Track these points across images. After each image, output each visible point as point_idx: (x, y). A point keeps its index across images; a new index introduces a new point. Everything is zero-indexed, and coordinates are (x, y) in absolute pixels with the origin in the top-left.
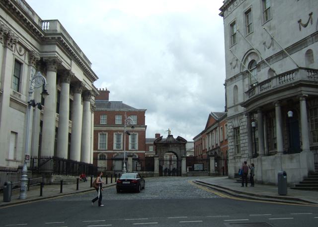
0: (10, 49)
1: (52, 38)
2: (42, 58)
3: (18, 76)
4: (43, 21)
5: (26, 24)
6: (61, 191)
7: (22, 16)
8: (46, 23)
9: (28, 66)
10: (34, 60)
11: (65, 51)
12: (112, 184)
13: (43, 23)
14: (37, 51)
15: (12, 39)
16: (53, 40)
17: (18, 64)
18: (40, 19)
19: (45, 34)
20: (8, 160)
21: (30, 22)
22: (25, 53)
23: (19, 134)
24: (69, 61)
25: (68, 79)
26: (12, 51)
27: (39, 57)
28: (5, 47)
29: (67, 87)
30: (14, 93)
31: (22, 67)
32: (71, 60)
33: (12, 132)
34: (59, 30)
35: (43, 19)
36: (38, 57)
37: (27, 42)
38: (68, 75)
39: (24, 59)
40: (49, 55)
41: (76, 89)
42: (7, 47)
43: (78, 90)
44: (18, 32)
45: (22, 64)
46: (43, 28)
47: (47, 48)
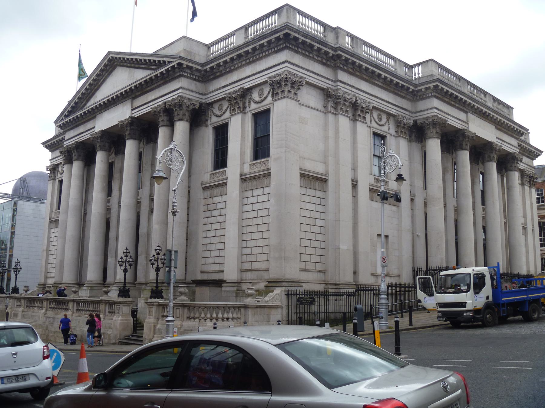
0: (362, 122)
1: (427, 89)
2: (415, 122)
5: (381, 81)
8: (417, 68)
9: (325, 113)
10: (404, 127)
15: (363, 108)
16: (428, 92)
18: (406, 65)
19: (415, 85)
22: (388, 120)
24: (462, 116)
25: (464, 143)
26: (366, 123)
29: (465, 156)
32: (466, 112)
33: (378, 235)
34: (436, 72)
35: (411, 64)
36: (410, 121)
37: (388, 105)
38: (514, 160)
39: (389, 129)
40: (426, 114)
41: (486, 156)
42: (356, 120)
43: (489, 157)
44: (372, 95)
45: (386, 136)
46: (414, 76)
47: (422, 105)
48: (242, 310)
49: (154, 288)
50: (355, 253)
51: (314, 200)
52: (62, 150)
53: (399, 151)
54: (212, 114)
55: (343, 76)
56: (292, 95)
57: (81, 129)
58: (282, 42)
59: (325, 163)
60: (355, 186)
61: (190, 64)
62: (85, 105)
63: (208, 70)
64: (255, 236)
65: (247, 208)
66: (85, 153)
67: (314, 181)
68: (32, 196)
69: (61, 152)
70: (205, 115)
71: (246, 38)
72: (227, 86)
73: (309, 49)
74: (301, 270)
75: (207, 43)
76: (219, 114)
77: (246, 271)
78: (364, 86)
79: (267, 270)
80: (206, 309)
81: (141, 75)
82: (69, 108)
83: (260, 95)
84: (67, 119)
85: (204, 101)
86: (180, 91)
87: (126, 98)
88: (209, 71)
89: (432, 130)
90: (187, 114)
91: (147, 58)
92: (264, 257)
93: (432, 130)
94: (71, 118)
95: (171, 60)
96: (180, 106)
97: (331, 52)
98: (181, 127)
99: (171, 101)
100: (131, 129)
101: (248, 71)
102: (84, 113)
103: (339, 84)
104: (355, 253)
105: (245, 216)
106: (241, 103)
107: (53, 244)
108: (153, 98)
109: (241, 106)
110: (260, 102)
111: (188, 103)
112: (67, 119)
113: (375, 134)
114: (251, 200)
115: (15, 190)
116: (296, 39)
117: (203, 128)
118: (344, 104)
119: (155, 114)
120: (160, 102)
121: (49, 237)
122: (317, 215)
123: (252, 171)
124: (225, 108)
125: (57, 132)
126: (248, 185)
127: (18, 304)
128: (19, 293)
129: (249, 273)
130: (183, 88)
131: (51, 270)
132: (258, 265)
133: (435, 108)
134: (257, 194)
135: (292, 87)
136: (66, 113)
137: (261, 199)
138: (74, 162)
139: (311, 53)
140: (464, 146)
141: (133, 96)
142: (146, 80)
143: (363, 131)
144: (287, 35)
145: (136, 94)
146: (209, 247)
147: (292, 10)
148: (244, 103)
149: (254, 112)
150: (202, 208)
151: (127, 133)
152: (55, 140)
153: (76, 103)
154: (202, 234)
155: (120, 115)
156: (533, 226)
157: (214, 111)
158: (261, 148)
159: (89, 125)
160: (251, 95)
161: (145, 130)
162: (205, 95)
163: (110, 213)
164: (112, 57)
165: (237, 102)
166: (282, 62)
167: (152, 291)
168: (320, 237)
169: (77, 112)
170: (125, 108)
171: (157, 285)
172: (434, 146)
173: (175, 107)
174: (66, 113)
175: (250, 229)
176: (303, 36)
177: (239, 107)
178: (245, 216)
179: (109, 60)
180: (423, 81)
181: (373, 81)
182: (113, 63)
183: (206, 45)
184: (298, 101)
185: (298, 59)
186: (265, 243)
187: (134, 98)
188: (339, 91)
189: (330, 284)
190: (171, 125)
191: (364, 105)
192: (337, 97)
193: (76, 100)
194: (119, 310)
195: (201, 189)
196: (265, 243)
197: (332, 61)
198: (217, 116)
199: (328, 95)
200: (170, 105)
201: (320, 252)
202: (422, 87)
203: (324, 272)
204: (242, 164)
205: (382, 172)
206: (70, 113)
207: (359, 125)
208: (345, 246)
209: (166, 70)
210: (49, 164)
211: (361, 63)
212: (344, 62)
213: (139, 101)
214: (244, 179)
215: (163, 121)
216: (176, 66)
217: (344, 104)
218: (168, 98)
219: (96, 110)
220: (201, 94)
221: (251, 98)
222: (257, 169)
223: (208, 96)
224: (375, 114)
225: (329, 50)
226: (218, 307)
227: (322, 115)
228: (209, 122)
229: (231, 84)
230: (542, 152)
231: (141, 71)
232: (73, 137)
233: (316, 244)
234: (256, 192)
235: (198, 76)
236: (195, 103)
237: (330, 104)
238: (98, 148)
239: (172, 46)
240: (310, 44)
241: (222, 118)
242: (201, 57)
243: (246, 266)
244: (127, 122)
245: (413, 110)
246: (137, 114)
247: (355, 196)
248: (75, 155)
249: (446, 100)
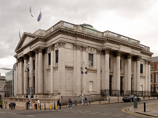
39: (94, 52)
50: (82, 85)
51: (70, 73)
53: (97, 58)
55: (78, 39)
61: (41, 37)
65: (54, 75)
67: (70, 68)
78: (86, 41)
88: (46, 40)
96: (39, 49)
97: (74, 33)
98: (40, 54)
101: (54, 39)
103: (77, 41)
104: (82, 85)
113: (89, 54)
114: (55, 73)
117: (46, 54)
133: (108, 45)
138: (39, 53)
144: (60, 30)
146: (48, 85)
147: (63, 22)
148: (53, 48)
150: (47, 75)
154: (46, 82)
156: (148, 74)
159: (22, 52)
163: (35, 75)
168: (71, 83)
169: (19, 49)
172: (107, 56)
182: (25, 36)
185: (64, 36)
187: (30, 46)
191: (85, 47)
201: (72, 86)
204: (53, 64)
208: (79, 84)
213: (32, 47)
218: (37, 47)
224: (90, 49)
226: (45, 100)
227: (73, 50)
230: (153, 53)
233: (70, 84)
238: (24, 59)
242: (44, 34)
243: (55, 90)
246: (32, 50)
248: (20, 60)
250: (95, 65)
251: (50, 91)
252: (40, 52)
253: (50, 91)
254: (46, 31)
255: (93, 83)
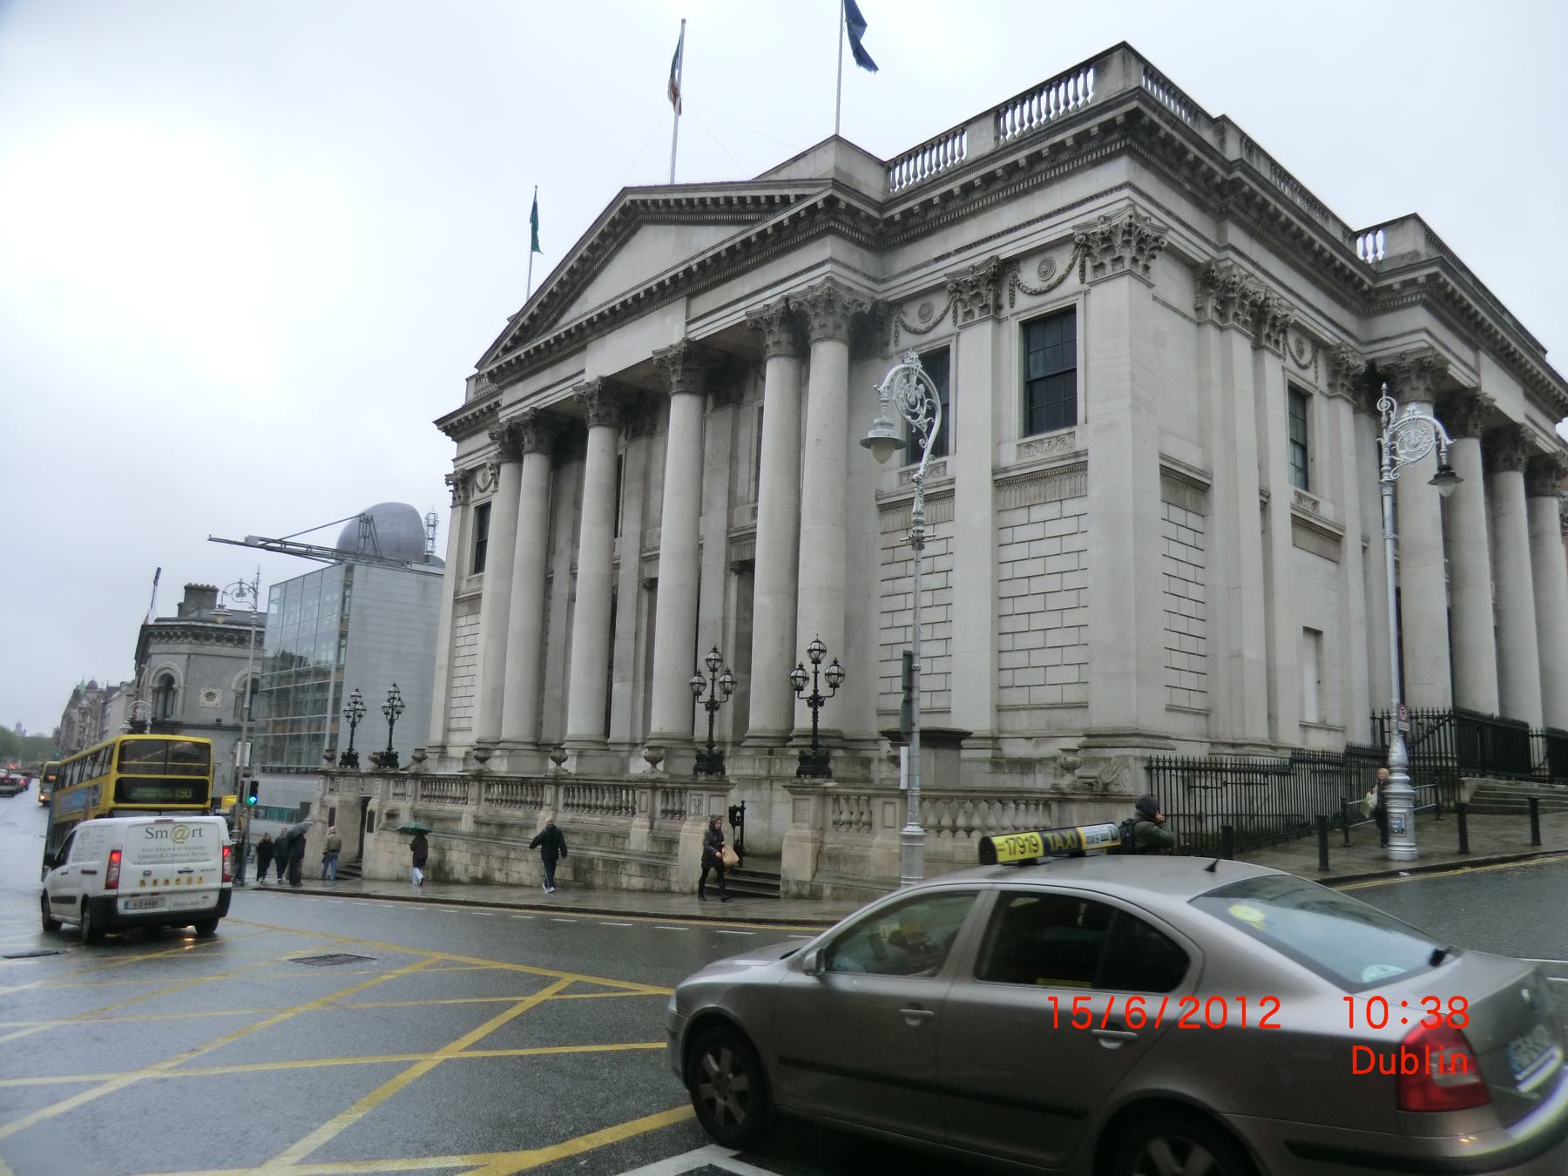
0: (1273, 353)
1: (1405, 284)
2: (1372, 364)
3: (1300, 440)
4: (1356, 235)
6: (1464, 849)
7: (1300, 233)
8: (1370, 237)
9: (1199, 324)
10: (1346, 376)
11: (1445, 313)
12: (658, 815)
13: (1360, 241)
14: (1351, 342)
15: (1275, 318)
17: (1299, 397)
20: (1305, 726)
21: (1326, 245)
22: (1315, 357)
23: (1326, 636)
24: (1467, 354)
25: (1471, 423)
27: (1361, 364)
28: (1257, 347)
30: (1300, 496)
31: (1309, 407)
33: (1307, 630)
39: (1316, 378)
40: (1396, 347)
41: (1501, 457)
43: (1508, 459)
44: (810, 269)
45: (1310, 395)
47: (1387, 324)
48: (1054, 807)
49: (809, 752)
52: (496, 429)
54: (901, 329)
56: (1140, 271)
57: (545, 378)
58: (1115, 136)
59: (1202, 445)
60: (1264, 506)
61: (855, 203)
62: (556, 321)
63: (897, 218)
64: (1038, 622)
66: (559, 436)
68: (385, 554)
69: (491, 436)
70: (882, 330)
71: (997, 138)
72: (948, 255)
73: (1173, 159)
74: (1170, 709)
75: (885, 159)
76: (922, 327)
77: (1015, 709)
79: (1083, 706)
80: (955, 804)
81: (710, 239)
82: (515, 331)
83: (1044, 274)
84: (511, 357)
85: (879, 297)
86: (827, 267)
87: (671, 294)
89: (1415, 383)
90: (844, 327)
91: (734, 194)
92: (1071, 674)
93: (1415, 383)
94: (520, 352)
95: (807, 191)
98: (828, 357)
99: (803, 293)
100: (684, 370)
102: (555, 338)
105: (1007, 571)
106: (991, 297)
107: (464, 651)
108: (748, 290)
109: (991, 302)
110: (1045, 292)
111: (847, 298)
112: (511, 357)
115: (344, 540)
116: (1153, 127)
118: (1242, 306)
119: (755, 329)
120: (772, 298)
121: (453, 638)
122: (1189, 572)
123: (1026, 460)
124: (937, 313)
125: (472, 397)
126: (1012, 496)
127: (398, 791)
128: (396, 765)
129: (1023, 714)
130: (835, 262)
131: (458, 713)
132: (1051, 695)
133: (1412, 330)
134: (1044, 518)
135: (1140, 250)
136: (507, 341)
137: (1053, 529)
138: (526, 457)
139: (1176, 171)
140: (1470, 428)
141: (690, 290)
142: (733, 246)
143: (1275, 373)
145: (702, 285)
148: (997, 297)
149: (1025, 317)
151: (674, 379)
152: (469, 413)
153: (532, 318)
155: (660, 333)
157: (908, 321)
158: (1049, 397)
160: (1015, 276)
161: (722, 372)
162: (884, 281)
164: (633, 202)
165: (978, 295)
166: (1108, 189)
167: (803, 759)
169: (536, 336)
170: (668, 320)
171: (815, 742)
173: (814, 306)
174: (507, 341)
175: (1022, 605)
176: (1168, 122)
177: (986, 306)
178: (1007, 571)
179: (624, 210)
180: (1387, 268)
181: (1293, 256)
182: (630, 215)
183: (881, 163)
184: (1150, 286)
186: (1071, 637)
187: (691, 296)
188: (1235, 271)
189: (1224, 744)
190: (801, 354)
192: (1228, 287)
193: (534, 309)
194: (698, 807)
195: (875, 511)
196: (1071, 637)
197: (1216, 197)
198: (915, 332)
199: (1204, 278)
200: (801, 304)
201: (1198, 664)
202: (1395, 282)
203: (1206, 714)
204: (459, 578)
205: (1386, 461)
206: (517, 341)
207: (1270, 361)
208: (1253, 652)
209: (791, 218)
210: (450, 469)
211: (1279, 207)
212: (1242, 202)
213: (703, 304)
214: (1003, 482)
215: (777, 343)
216: (820, 205)
217: (1242, 306)
218: (797, 286)
219: (588, 331)
220: (874, 280)
221: (1017, 284)
222: (1038, 456)
223: (893, 284)
225: (1216, 168)
227: (1192, 327)
228: (892, 348)
229: (958, 251)
231: (711, 229)
232: (518, 401)
234: (1038, 513)
235: (868, 235)
236: (861, 300)
237: (1211, 304)
239: (802, 162)
240: (1181, 145)
241: (931, 336)
243: (1012, 697)
244: (674, 352)
245: (1363, 338)
246: (701, 332)
247: (1266, 531)
248: (528, 440)
249: (1445, 313)
250: (1327, 493)
251: (947, 711)
252: (828, 338)
253: (947, 711)
254: (888, 167)
255: (1319, 649)
